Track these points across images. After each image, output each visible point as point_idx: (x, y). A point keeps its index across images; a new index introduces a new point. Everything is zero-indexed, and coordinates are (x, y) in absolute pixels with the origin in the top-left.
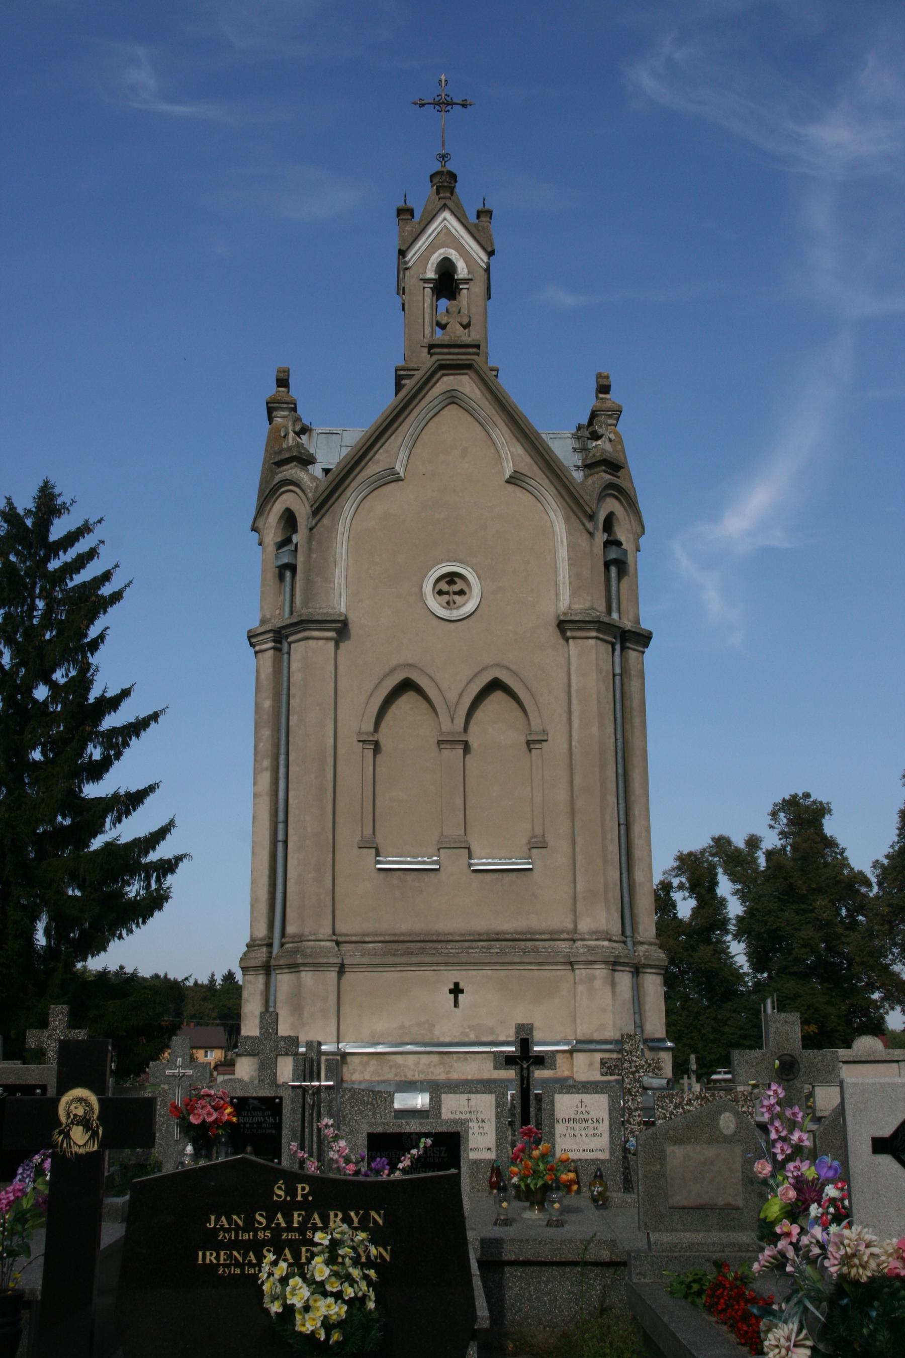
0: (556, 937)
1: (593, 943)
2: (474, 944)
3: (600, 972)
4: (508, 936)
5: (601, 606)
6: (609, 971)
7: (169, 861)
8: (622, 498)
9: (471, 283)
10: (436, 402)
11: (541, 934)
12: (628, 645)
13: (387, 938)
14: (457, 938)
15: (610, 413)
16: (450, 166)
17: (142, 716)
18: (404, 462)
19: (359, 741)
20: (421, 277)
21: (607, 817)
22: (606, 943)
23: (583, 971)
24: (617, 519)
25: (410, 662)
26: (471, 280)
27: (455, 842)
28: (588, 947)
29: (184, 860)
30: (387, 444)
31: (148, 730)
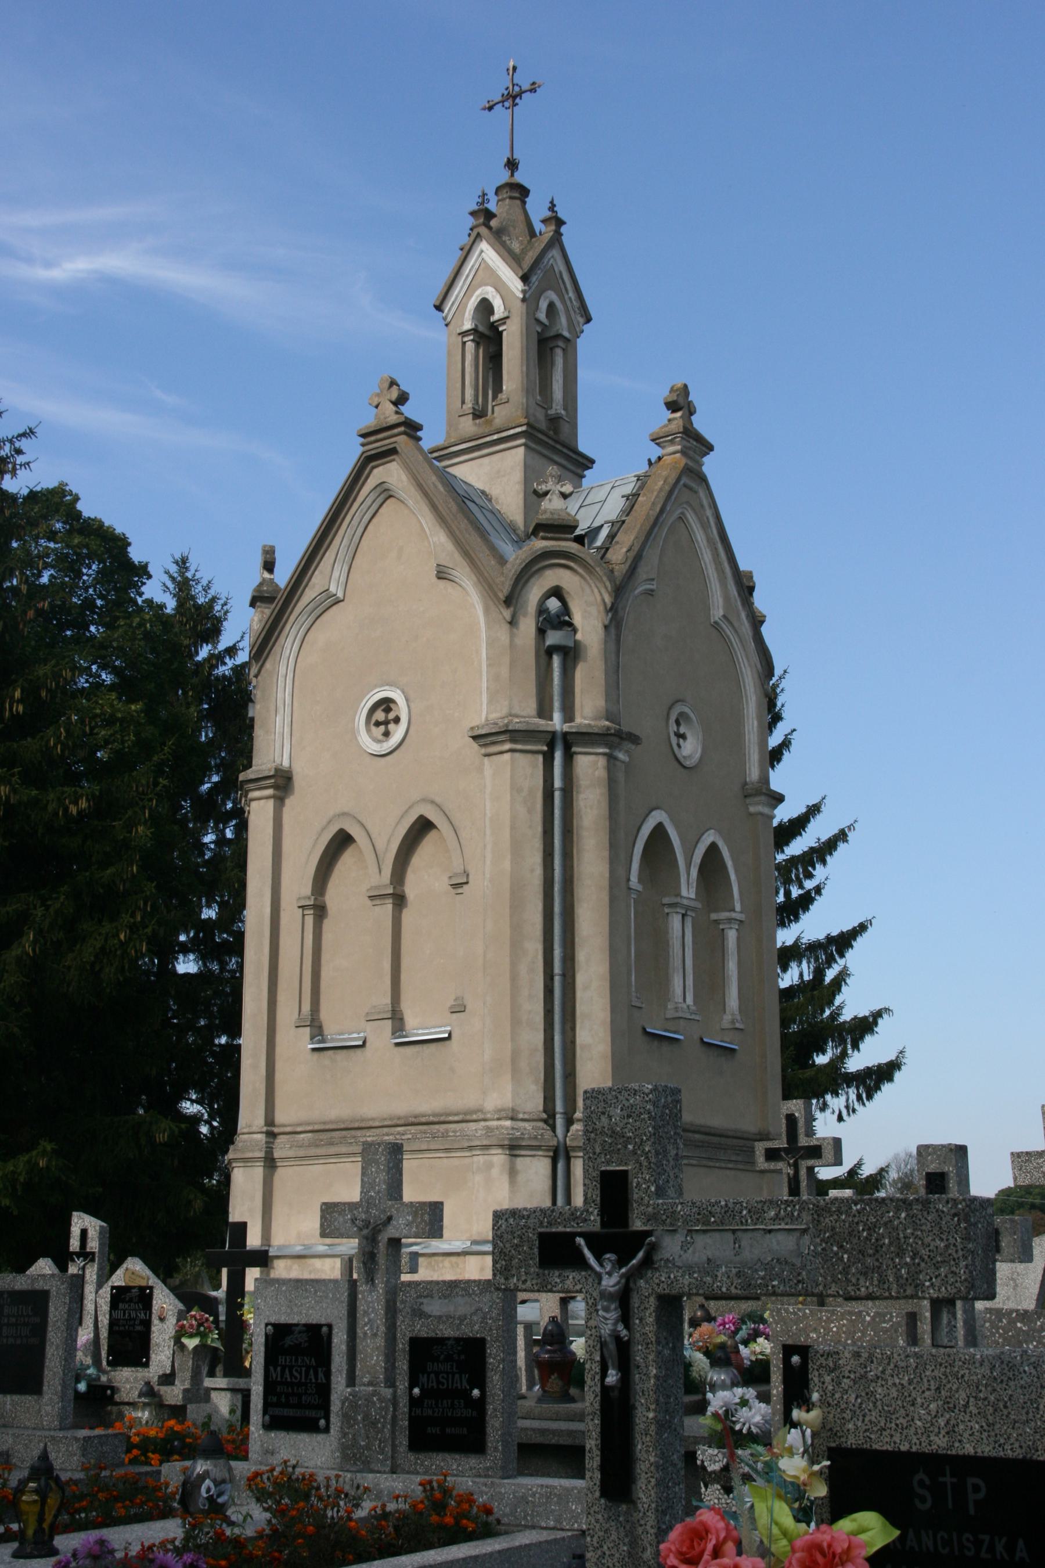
0: (468, 1117)
1: (495, 1123)
2: (393, 1130)
3: (499, 1158)
4: (423, 1120)
5: (530, 707)
6: (507, 1156)
7: (865, 1018)
8: (572, 564)
9: (508, 321)
10: (369, 501)
11: (456, 1114)
12: (574, 749)
13: (317, 1127)
14: (377, 1124)
15: (670, 438)
16: (520, 177)
17: (823, 839)
18: (343, 579)
19: (299, 907)
20: (459, 331)
21: (523, 969)
22: (508, 1123)
23: (480, 1157)
24: (568, 593)
25: (346, 810)
26: (507, 318)
27: (379, 1013)
28: (488, 1128)
29: (885, 1016)
30: (322, 564)
31: (835, 854)
